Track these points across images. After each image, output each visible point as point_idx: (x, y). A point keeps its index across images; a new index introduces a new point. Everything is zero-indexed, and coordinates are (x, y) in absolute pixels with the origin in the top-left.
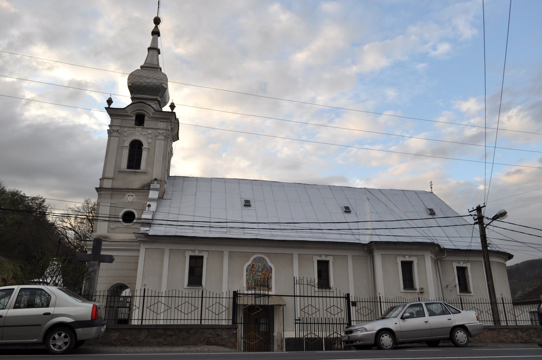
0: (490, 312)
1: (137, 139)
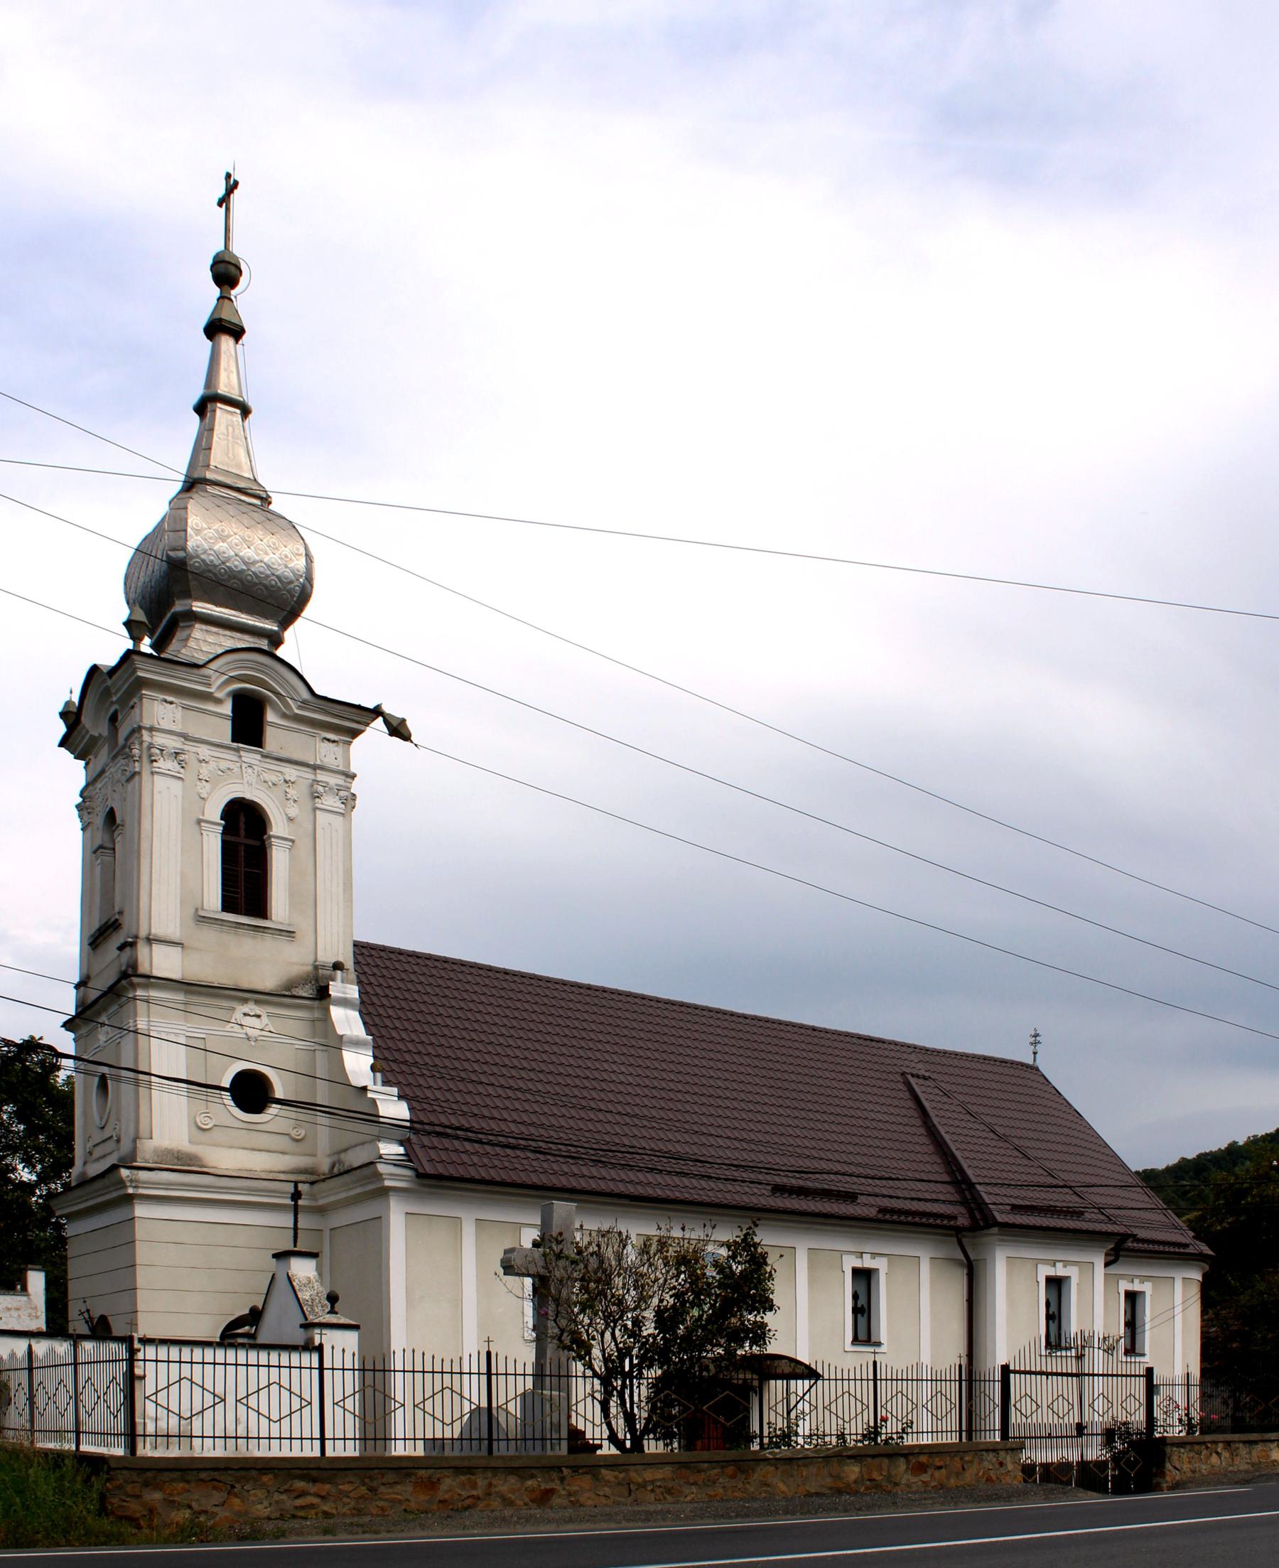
1: (248, 796)
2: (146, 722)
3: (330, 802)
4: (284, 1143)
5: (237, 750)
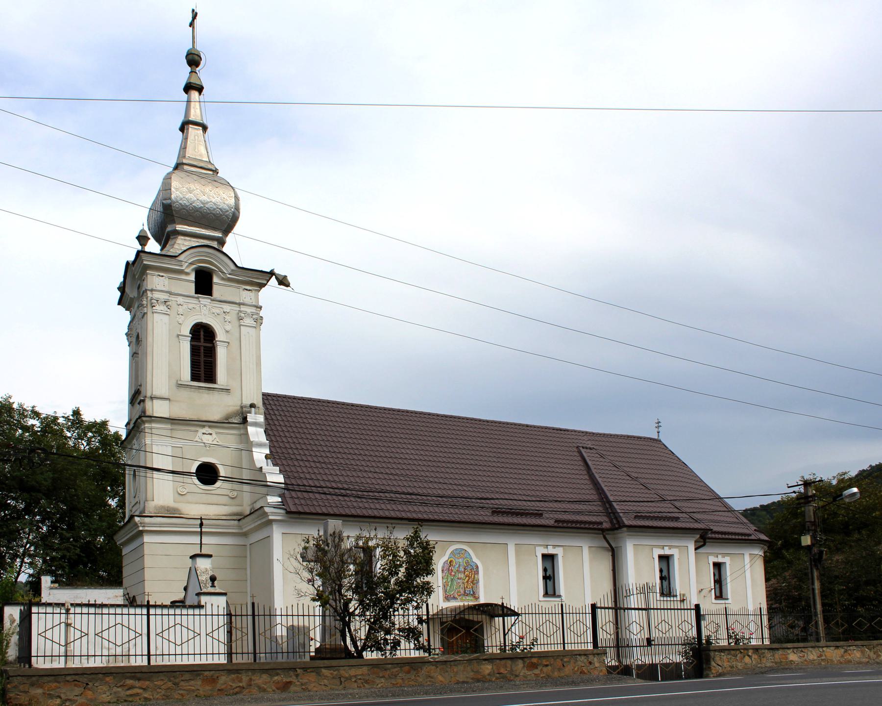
0: (222, 635)
1: (204, 321)
2: (149, 287)
3: (248, 321)
4: (225, 500)
5: (198, 298)
